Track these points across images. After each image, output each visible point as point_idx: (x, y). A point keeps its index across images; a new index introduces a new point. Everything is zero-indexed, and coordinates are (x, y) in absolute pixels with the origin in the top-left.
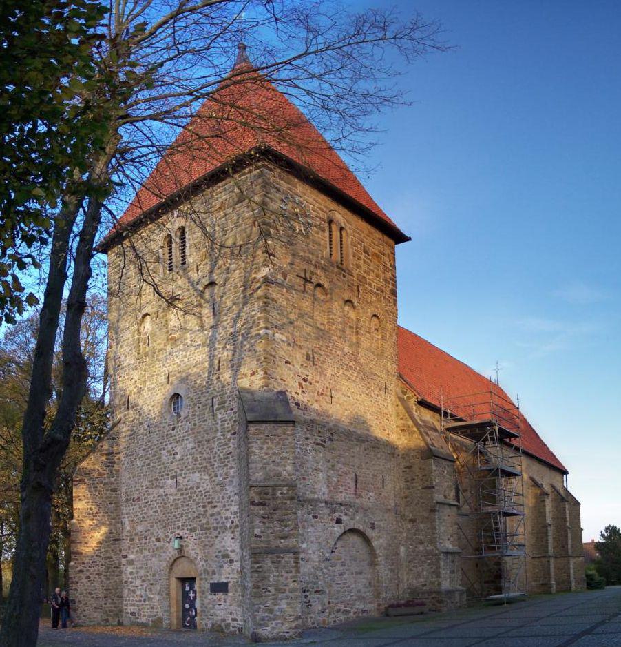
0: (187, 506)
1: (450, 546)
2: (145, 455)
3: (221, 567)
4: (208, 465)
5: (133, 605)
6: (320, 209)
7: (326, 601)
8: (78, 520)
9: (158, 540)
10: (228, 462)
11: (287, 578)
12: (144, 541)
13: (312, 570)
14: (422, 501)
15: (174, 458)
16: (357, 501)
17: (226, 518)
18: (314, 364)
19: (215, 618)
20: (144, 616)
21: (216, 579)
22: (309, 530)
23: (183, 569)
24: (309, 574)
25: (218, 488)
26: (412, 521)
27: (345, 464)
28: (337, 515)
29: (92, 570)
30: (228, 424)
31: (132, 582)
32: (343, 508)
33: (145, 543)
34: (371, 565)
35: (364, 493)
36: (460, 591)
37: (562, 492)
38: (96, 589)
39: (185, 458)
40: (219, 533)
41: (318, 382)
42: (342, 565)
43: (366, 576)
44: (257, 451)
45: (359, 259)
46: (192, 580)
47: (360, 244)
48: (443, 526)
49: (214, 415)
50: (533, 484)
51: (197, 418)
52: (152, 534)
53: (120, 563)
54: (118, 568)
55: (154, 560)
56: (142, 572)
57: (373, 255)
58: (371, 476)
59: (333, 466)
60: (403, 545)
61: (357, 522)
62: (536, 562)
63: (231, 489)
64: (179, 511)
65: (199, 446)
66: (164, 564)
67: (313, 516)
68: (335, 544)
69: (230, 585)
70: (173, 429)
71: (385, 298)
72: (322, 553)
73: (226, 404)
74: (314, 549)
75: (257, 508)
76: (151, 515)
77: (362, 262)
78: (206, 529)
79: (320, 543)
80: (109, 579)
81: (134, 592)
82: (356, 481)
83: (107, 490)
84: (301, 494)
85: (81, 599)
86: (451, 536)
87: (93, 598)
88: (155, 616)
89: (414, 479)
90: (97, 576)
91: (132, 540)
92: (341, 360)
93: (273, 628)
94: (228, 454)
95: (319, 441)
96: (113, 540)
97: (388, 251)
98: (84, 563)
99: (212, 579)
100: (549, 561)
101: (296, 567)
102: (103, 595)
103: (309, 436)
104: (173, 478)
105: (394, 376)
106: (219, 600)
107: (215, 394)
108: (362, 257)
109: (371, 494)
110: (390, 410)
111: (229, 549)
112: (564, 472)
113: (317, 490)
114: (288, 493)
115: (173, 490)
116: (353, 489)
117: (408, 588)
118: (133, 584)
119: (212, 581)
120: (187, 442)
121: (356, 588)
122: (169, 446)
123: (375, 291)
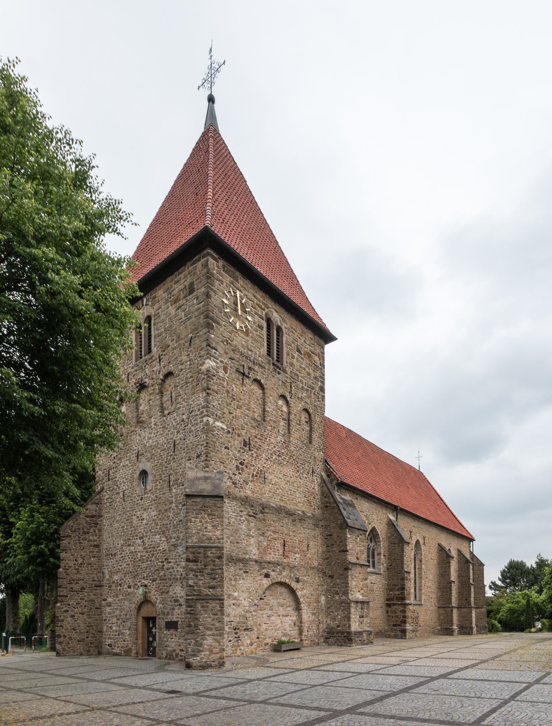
0: (151, 561)
1: (361, 597)
2: (121, 519)
3: (174, 609)
4: (166, 530)
5: (111, 639)
7: (254, 637)
8: (64, 569)
9: (129, 587)
10: (180, 528)
11: (213, 620)
12: (119, 588)
13: (243, 613)
14: (339, 561)
15: (141, 523)
16: (285, 560)
17: (178, 571)
18: (250, 450)
19: (169, 649)
20: (118, 647)
21: (170, 618)
23: (146, 611)
24: (240, 616)
25: (172, 548)
26: (331, 577)
27: (274, 532)
28: (265, 571)
29: (76, 610)
30: (180, 497)
31: (109, 620)
32: (270, 565)
33: (120, 590)
34: (296, 610)
35: (291, 555)
36: (367, 631)
37: (468, 556)
38: (80, 626)
39: (150, 523)
40: (172, 583)
41: (254, 466)
42: (270, 610)
43: (292, 618)
44: (193, 519)
45: (293, 357)
46: (153, 619)
48: (355, 581)
49: (170, 490)
50: (441, 549)
51: (158, 491)
52: (125, 582)
53: (101, 605)
54: (99, 608)
55: (126, 602)
56: (117, 612)
58: (298, 542)
59: (263, 533)
60: (324, 595)
61: (285, 577)
62: (442, 611)
63: (181, 549)
64: (144, 565)
65: (159, 514)
66: (133, 606)
67: (244, 572)
68: (264, 593)
69: (179, 623)
70: (141, 499)
71: (314, 394)
72: (252, 600)
73: (179, 481)
74: (245, 597)
75: (192, 564)
76: (125, 567)
77: (295, 360)
78: (163, 579)
80: (91, 618)
81: (111, 628)
82: (284, 546)
83: (91, 546)
84: (234, 554)
85: (66, 634)
86: (362, 589)
87: (76, 633)
88: (127, 646)
89: (333, 545)
90: (80, 615)
91: (110, 586)
92: (275, 447)
93: (202, 659)
94: (180, 521)
95: (251, 514)
96: (95, 586)
97: (318, 351)
98: (69, 605)
99: (167, 618)
100: (452, 611)
101: (221, 610)
102: (86, 630)
103: (243, 509)
104: (140, 538)
105: (321, 461)
106: (172, 635)
107: (172, 472)
108: (296, 356)
109: (297, 555)
110: (317, 490)
111: (179, 595)
112: (470, 540)
113: (249, 552)
115: (141, 548)
116: (281, 552)
117: (327, 628)
118: (111, 622)
119: (167, 620)
120: (151, 510)
121: (282, 627)
122: (138, 513)
123: (306, 387)
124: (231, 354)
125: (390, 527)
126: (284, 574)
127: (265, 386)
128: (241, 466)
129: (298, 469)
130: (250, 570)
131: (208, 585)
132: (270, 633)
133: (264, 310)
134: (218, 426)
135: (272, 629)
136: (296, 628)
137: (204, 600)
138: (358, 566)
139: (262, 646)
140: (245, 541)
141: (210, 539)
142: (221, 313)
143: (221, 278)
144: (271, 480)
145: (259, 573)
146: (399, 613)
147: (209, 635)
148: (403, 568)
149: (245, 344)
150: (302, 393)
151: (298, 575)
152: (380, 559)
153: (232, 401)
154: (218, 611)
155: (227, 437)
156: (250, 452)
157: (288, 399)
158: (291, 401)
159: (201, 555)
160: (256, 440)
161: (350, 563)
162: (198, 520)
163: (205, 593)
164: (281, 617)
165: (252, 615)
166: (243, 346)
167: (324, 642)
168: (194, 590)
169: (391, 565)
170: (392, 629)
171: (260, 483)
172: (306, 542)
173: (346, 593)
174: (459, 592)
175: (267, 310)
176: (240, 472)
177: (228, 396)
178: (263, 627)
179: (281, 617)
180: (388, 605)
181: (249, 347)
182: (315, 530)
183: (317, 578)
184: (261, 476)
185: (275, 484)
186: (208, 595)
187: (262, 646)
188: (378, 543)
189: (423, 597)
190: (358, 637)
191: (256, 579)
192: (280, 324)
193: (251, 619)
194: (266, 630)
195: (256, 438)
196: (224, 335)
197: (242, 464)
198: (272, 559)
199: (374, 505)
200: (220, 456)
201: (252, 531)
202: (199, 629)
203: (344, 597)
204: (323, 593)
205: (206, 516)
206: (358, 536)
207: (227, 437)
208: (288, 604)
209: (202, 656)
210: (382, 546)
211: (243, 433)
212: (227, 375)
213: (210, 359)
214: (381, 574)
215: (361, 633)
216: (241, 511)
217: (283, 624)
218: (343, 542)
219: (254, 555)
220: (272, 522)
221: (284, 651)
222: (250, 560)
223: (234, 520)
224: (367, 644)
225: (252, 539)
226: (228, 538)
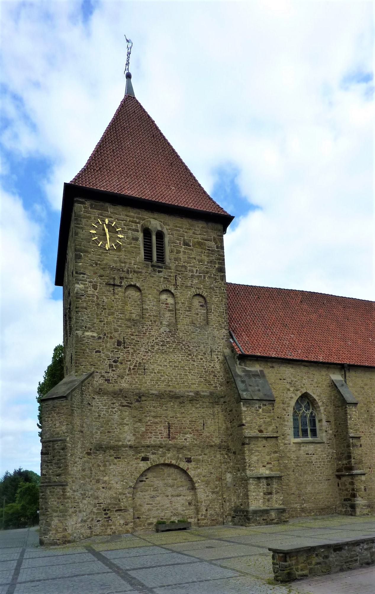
6: (132, 222)
11: (58, 503)
13: (114, 495)
18: (124, 348)
24: (111, 498)
41: (130, 361)
43: (185, 498)
45: (178, 252)
59: (140, 420)
71: (209, 277)
72: (126, 483)
93: (50, 537)
95: (125, 404)
101: (63, 495)
103: (115, 401)
105: (223, 339)
110: (218, 368)
114: (61, 445)
124: (101, 272)
125: (333, 389)
126: (169, 455)
128: (114, 364)
131: (55, 473)
132: (154, 513)
133: (139, 223)
134: (88, 336)
135: (158, 509)
138: (260, 439)
139: (144, 526)
140: (118, 430)
143: (88, 215)
144: (153, 369)
146: (348, 486)
147: (55, 517)
148: (347, 433)
149: (118, 259)
150: (192, 282)
152: (321, 426)
153: (102, 311)
155: (98, 343)
156: (126, 350)
157: (172, 291)
158: (177, 293)
159: (51, 448)
160: (132, 337)
161: (245, 437)
163: (54, 480)
164: (170, 497)
165: (126, 497)
166: (115, 262)
167: (232, 521)
168: (46, 478)
169: (337, 432)
170: (343, 504)
171: (139, 374)
173: (244, 470)
176: (114, 369)
177: (97, 308)
180: (339, 477)
181: (122, 260)
182: (213, 407)
183: (218, 456)
184: (140, 368)
185: (158, 372)
186: (55, 482)
187: (144, 526)
188: (318, 409)
190: (261, 516)
191: (131, 463)
192: (160, 229)
194: (149, 510)
195: (132, 335)
196: (93, 259)
197: (115, 362)
198: (152, 442)
199: (305, 370)
200: (91, 360)
203: (243, 474)
205: (55, 415)
206: (260, 407)
207: (98, 343)
208: (180, 484)
209: (50, 535)
210: (322, 411)
212: (97, 291)
213: (78, 283)
214: (323, 443)
216: (113, 403)
217: (173, 504)
218: (239, 414)
219: (129, 441)
220: (152, 408)
221: (163, 531)
223: (105, 412)
225: (126, 428)
226: (97, 429)
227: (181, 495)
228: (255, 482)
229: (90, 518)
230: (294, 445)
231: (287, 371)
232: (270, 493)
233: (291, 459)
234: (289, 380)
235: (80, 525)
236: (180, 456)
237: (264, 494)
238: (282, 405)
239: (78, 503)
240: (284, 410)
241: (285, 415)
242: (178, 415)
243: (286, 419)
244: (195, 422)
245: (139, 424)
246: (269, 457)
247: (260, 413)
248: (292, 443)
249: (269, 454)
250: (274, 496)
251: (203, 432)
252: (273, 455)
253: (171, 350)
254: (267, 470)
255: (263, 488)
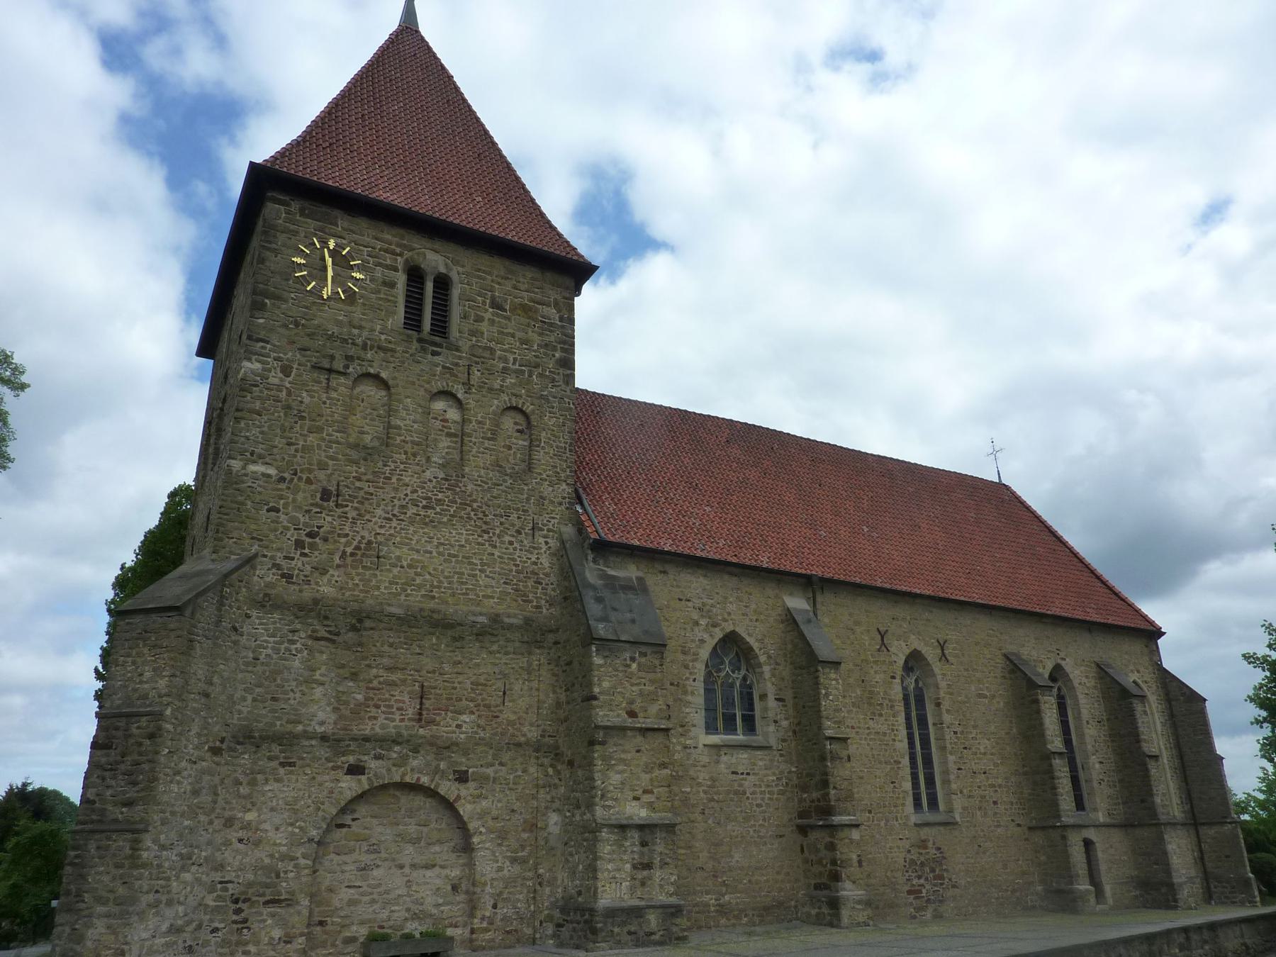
1: (643, 813)
11: (114, 879)
13: (267, 861)
16: (421, 731)
18: (337, 506)
22: (267, 788)
27: (389, 669)
28: (351, 759)
42: (368, 852)
43: (447, 871)
47: (484, 296)
57: (513, 310)
60: (557, 810)
62: (1038, 838)
79: (295, 812)
95: (322, 633)
100: (1064, 838)
103: (299, 626)
105: (560, 504)
108: (487, 316)
109: (465, 717)
114: (148, 727)
126: (415, 763)
127: (390, 382)
129: (485, 527)
130: (303, 759)
133: (401, 255)
136: (461, 897)
137: (103, 831)
138: (629, 733)
139: (333, 945)
141: (145, 697)
142: (288, 280)
145: (331, 764)
146: (824, 853)
147: (100, 916)
151: (463, 763)
154: (126, 858)
156: (339, 511)
161: (597, 727)
162: (130, 659)
163: (114, 816)
164: (407, 870)
165: (296, 866)
166: (339, 324)
168: (93, 811)
169: (799, 724)
172: (500, 684)
173: (590, 806)
174: (1121, 781)
175: (407, 254)
176: (306, 551)
178: (342, 896)
179: (407, 870)
180: (803, 830)
182: (530, 653)
183: (532, 770)
185: (410, 566)
186: (116, 821)
188: (757, 670)
189: (958, 803)
190: (623, 924)
191: (319, 778)
193: (291, 875)
194: (352, 903)
195: (359, 479)
198: (378, 730)
199: (732, 582)
200: (253, 527)
201: (318, 672)
202: (83, 901)
204: (557, 805)
205: (146, 651)
206: (633, 659)
210: (767, 675)
211: (321, 475)
215: (635, 913)
216: (293, 631)
220: (386, 648)
222: (307, 735)
224: (661, 943)
227: (434, 866)
228: (613, 837)
229: (192, 921)
230: (706, 749)
231: (697, 584)
232: (648, 866)
233: (699, 784)
234: (698, 603)
235: (163, 940)
236: (443, 765)
237: (634, 867)
238: (681, 657)
239: (168, 879)
240: (686, 667)
241: (687, 679)
242: (447, 667)
243: (690, 689)
244: (485, 685)
245: (351, 684)
246: (648, 776)
247: (632, 673)
248: (701, 746)
249: (648, 769)
250: (657, 874)
251: (501, 711)
252: (657, 772)
253: (445, 519)
254: (643, 807)
255: (633, 852)
